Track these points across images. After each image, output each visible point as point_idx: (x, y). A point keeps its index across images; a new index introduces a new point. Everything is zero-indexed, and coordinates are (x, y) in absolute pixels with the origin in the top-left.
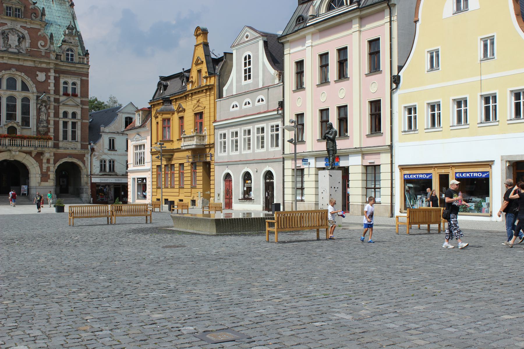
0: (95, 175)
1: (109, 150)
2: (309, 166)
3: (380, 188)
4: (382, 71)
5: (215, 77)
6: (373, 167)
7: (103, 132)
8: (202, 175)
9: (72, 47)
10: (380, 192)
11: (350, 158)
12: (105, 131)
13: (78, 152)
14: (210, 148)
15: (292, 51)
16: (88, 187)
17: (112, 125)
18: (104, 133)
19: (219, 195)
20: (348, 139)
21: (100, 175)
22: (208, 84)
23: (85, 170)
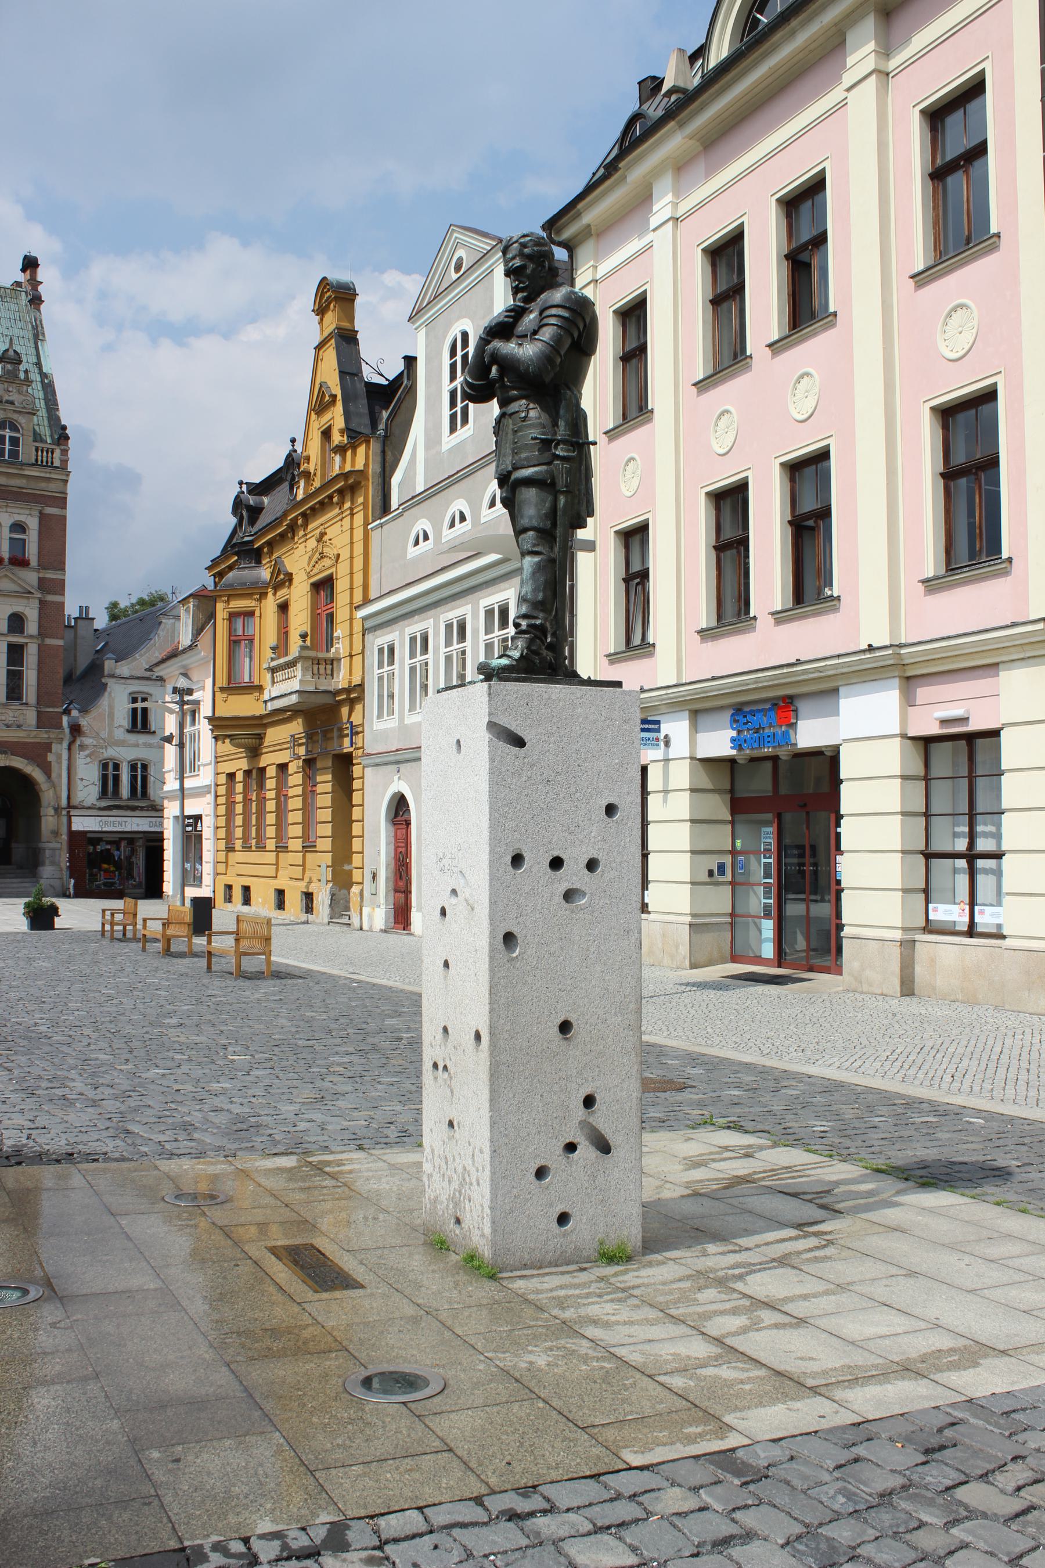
0: (83, 808)
1: (128, 731)
2: (666, 753)
3: (998, 856)
4: (1010, 560)
5: (368, 442)
6: (964, 742)
7: (112, 676)
8: (330, 804)
9: (15, 416)
10: (998, 873)
11: (843, 702)
12: (118, 672)
13: (29, 736)
14: (352, 703)
15: (604, 268)
16: (59, 846)
17: (141, 656)
18: (114, 680)
19: (374, 877)
20: (836, 609)
21: (100, 809)
22: (348, 468)
23: (51, 792)
